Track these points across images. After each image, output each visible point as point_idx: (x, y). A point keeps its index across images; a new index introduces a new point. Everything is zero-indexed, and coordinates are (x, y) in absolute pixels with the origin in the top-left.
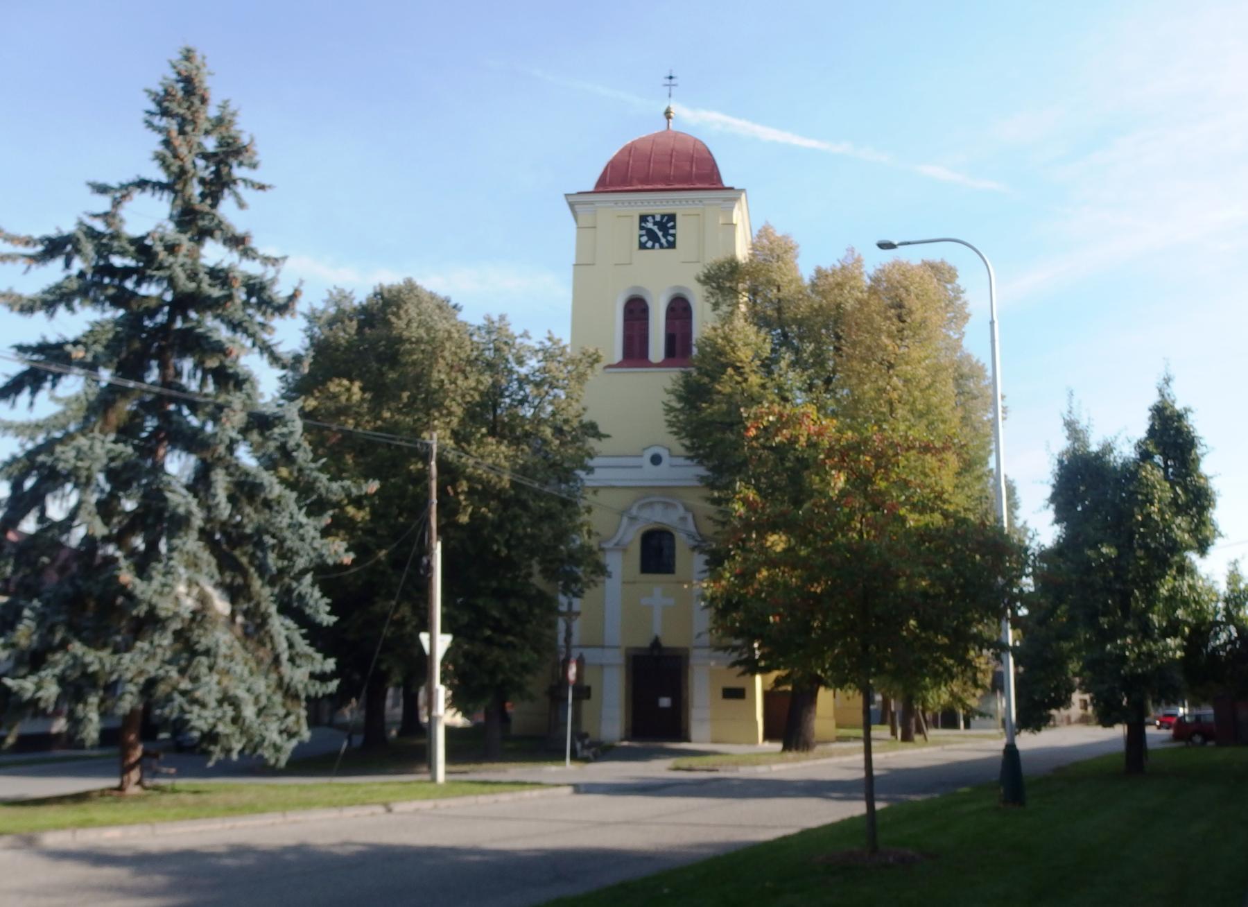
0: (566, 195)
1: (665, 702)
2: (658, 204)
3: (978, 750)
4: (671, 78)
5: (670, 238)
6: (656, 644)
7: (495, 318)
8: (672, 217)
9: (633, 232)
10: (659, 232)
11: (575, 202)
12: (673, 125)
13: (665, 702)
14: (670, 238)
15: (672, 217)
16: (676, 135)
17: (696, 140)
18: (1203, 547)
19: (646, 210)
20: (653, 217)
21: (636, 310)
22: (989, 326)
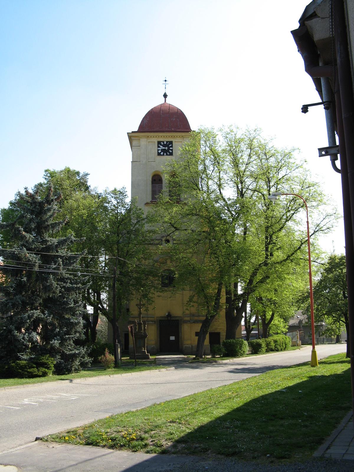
0: (128, 133)
1: (172, 338)
2: (165, 137)
3: (226, 364)
4: (166, 81)
5: (162, 153)
6: (169, 315)
7: (23, 192)
8: (171, 143)
9: (154, 149)
10: (167, 149)
11: (131, 136)
12: (169, 101)
13: (172, 338)
14: (162, 153)
15: (171, 143)
16: (170, 107)
17: (178, 109)
18: (41, 185)
19: (161, 139)
20: (163, 142)
21: (157, 179)
22: (306, 224)
